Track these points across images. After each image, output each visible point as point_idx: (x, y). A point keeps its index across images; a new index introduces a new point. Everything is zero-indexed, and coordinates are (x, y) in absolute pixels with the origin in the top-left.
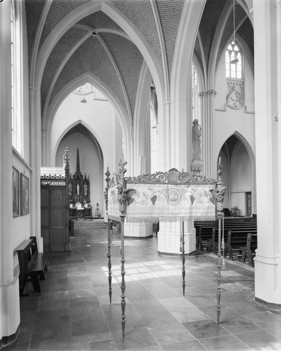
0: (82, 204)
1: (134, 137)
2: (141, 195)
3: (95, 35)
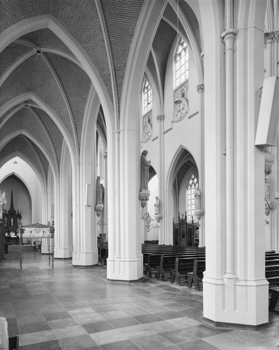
0: (15, 233)
1: (48, 192)
2: (27, 231)
3: (39, 54)
